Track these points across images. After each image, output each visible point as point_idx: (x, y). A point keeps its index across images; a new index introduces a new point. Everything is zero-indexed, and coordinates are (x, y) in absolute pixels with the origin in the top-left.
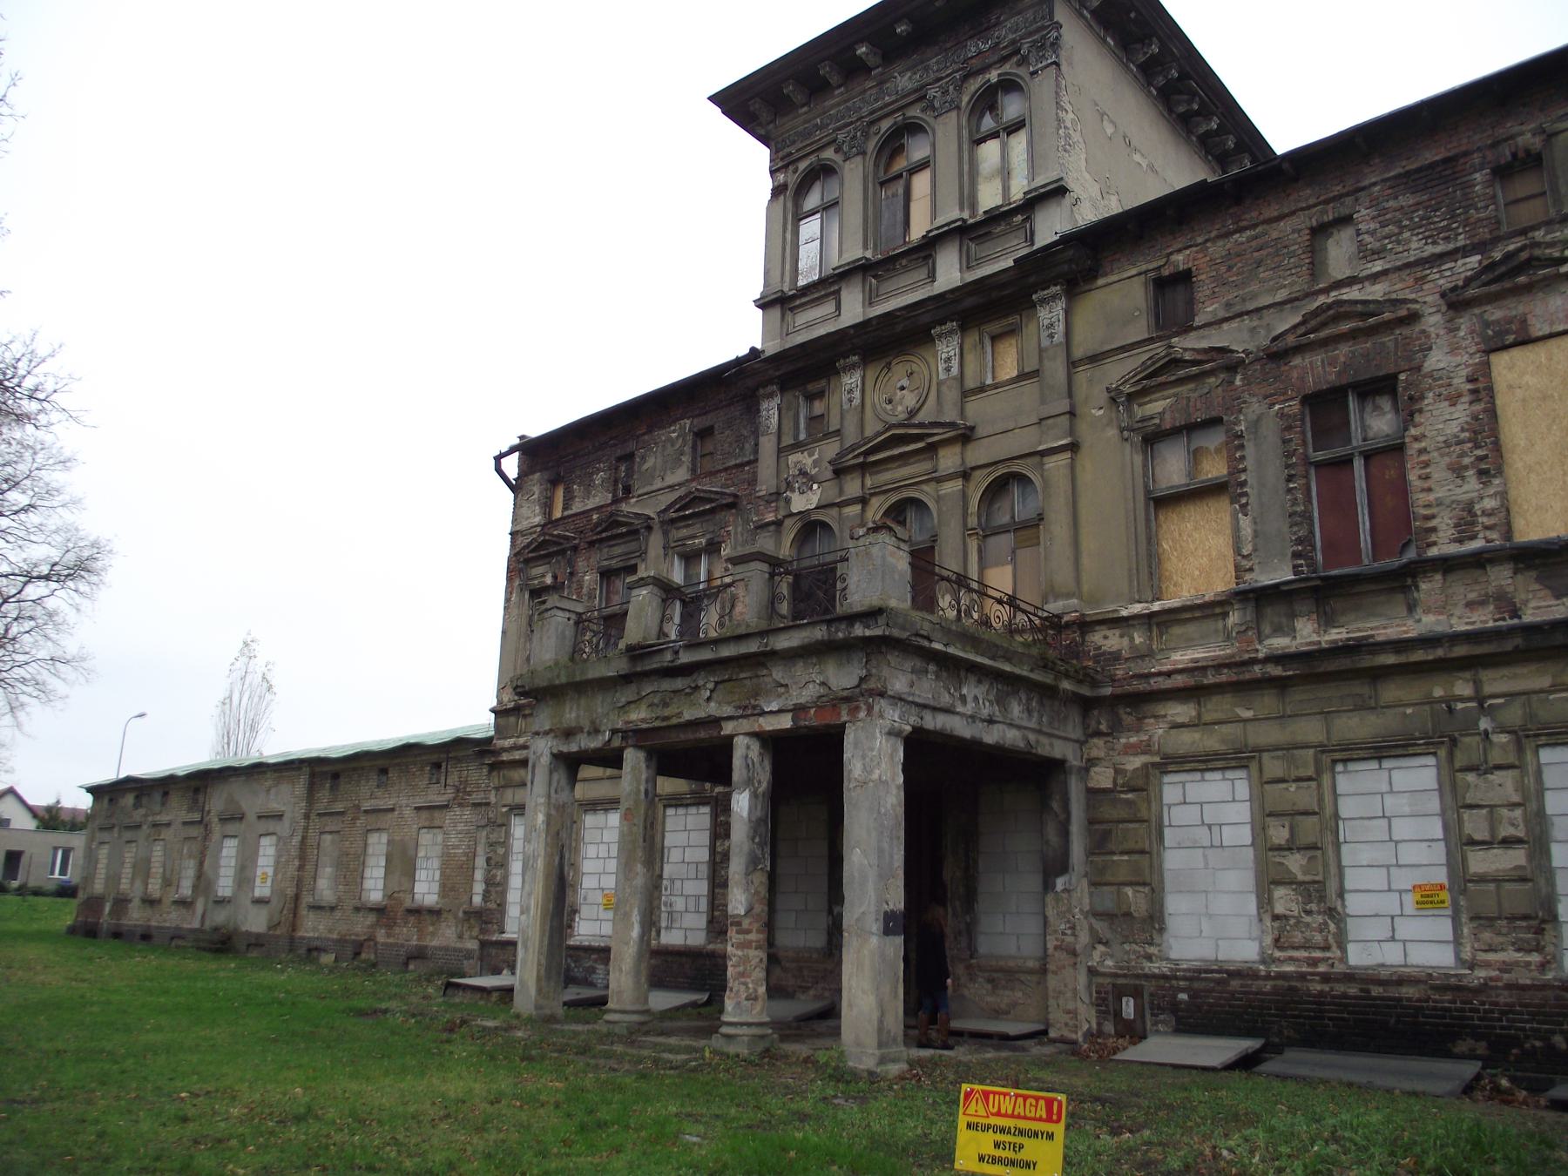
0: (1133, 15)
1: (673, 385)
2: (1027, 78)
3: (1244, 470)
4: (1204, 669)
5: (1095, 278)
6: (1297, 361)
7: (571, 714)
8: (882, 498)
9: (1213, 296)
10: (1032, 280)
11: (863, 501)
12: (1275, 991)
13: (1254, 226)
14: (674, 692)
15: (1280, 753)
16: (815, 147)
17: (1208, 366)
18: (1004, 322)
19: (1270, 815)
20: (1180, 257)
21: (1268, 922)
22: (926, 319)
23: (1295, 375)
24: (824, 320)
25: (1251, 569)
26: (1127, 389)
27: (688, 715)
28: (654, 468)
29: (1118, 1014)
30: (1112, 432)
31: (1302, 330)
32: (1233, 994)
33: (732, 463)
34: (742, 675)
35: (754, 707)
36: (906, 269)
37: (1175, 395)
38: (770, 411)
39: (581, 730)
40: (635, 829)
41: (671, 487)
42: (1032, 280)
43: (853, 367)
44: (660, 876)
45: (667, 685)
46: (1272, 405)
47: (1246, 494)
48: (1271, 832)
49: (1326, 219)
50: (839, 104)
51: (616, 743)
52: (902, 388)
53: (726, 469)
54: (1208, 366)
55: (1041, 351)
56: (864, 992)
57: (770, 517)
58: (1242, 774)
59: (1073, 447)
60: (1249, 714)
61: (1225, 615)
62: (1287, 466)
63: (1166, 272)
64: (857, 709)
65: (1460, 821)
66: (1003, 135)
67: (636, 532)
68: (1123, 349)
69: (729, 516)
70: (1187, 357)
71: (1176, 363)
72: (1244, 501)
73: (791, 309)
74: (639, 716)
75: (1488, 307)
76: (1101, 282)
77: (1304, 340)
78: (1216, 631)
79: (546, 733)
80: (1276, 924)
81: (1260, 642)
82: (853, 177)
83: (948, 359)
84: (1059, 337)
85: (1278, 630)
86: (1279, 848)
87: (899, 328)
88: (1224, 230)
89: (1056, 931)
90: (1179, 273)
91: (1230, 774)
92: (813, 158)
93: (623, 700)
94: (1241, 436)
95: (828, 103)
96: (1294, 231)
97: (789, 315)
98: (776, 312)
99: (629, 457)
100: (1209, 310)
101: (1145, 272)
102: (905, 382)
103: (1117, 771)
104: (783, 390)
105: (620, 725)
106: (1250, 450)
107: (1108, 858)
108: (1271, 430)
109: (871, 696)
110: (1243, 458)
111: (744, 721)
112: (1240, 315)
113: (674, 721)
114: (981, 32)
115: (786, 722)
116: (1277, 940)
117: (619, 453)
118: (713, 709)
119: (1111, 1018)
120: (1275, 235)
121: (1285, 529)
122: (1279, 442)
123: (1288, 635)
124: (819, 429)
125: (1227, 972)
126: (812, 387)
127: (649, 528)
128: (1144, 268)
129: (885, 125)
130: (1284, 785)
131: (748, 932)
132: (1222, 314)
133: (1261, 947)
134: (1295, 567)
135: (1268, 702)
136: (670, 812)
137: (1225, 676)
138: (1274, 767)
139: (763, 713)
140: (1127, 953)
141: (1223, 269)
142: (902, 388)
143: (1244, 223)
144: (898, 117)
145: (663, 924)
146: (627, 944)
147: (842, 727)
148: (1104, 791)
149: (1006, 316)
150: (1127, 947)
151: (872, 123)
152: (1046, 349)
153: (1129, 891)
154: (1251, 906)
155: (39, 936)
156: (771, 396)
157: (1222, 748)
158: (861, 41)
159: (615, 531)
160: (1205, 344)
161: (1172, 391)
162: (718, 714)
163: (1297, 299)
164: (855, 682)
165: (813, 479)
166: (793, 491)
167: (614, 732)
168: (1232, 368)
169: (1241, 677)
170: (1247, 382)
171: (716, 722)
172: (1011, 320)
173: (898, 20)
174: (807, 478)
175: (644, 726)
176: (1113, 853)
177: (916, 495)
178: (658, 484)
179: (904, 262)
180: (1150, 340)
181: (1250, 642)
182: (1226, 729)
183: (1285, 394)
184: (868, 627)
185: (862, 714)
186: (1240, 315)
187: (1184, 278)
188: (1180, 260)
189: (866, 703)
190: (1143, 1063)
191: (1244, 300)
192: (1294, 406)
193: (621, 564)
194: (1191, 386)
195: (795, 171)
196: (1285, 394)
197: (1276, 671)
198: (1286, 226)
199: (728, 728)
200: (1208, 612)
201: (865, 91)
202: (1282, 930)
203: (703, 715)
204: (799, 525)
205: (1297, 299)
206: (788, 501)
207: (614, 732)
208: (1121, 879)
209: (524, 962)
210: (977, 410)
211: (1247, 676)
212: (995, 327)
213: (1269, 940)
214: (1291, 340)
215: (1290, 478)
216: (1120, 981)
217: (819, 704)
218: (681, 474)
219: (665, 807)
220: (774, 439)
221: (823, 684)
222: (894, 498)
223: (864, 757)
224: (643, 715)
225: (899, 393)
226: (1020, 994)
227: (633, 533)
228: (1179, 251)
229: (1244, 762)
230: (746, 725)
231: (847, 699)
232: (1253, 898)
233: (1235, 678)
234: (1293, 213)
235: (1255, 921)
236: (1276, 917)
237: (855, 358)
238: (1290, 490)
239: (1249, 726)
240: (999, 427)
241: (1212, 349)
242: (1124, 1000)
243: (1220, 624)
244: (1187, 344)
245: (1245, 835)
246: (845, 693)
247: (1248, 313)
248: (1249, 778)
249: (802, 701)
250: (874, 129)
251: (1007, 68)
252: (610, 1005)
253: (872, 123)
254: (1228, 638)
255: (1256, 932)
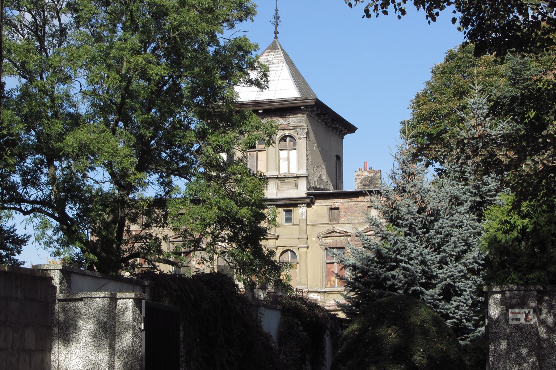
0: (209, 121)
1: (345, 120)
17: (342, 235)
20: (337, 204)
26: (322, 236)
30: (317, 245)
55: (299, 220)
59: (308, 248)
75: (279, 119)
84: (304, 217)
100: (342, 220)
132: (346, 222)
155: (100, 298)
244: (338, 228)
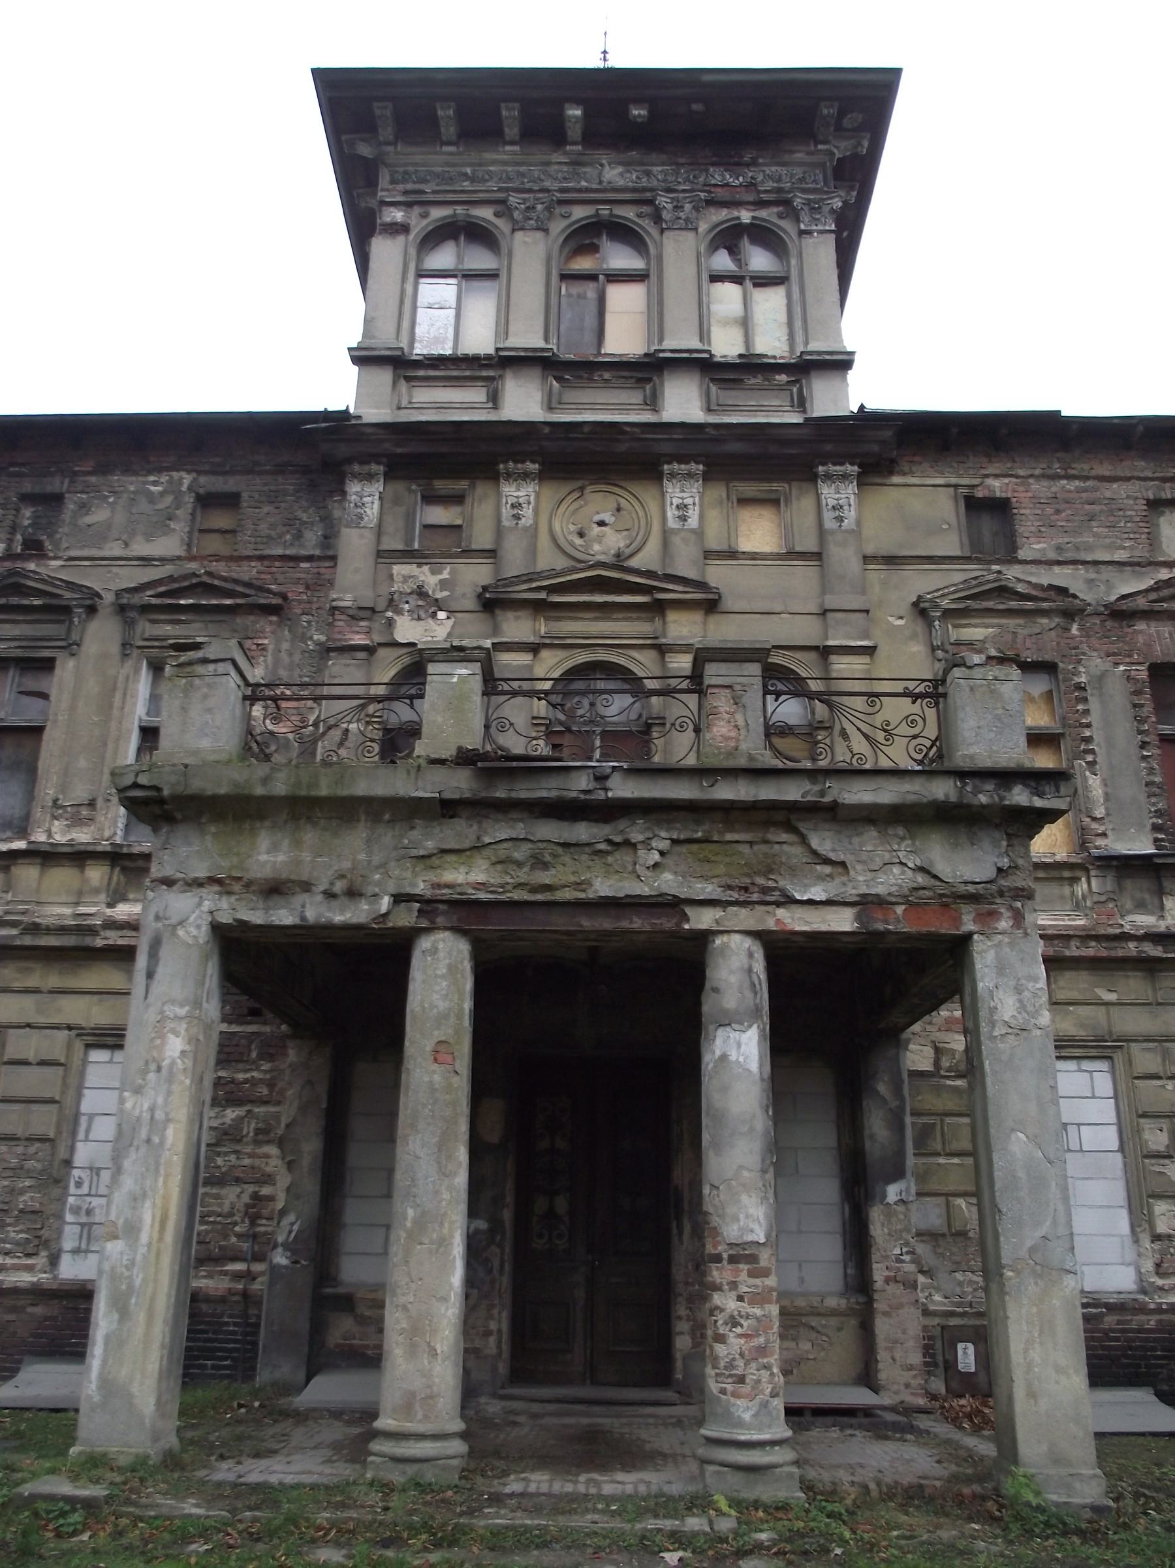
2: (794, 235)
3: (1089, 725)
4: (1068, 938)
5: (891, 473)
6: (1141, 626)
7: (268, 854)
8: (561, 654)
9: (1039, 534)
10: (828, 447)
11: (534, 649)
12: (1161, 1327)
13: (1087, 478)
14: (566, 845)
15: (1151, 1045)
16: (464, 197)
17: (1045, 605)
18: (765, 486)
19: (1144, 1115)
21: (1146, 1243)
22: (666, 448)
23: (1141, 639)
24: (470, 407)
25: (1104, 835)
26: (945, 603)
27: (603, 887)
28: (108, 525)
29: (950, 1366)
31: (1153, 596)
32: (1106, 1332)
33: (280, 552)
34: (729, 837)
35: (765, 890)
36: (607, 385)
37: (999, 626)
38: (367, 498)
39: (306, 887)
40: (456, 1080)
41: (146, 561)
42: (828, 447)
43: (525, 476)
44: (68, 1163)
45: (549, 830)
46: (1117, 664)
47: (1092, 752)
48: (1147, 1135)
49: (1164, 496)
50: (505, 163)
51: (406, 918)
52: (601, 524)
53: (261, 558)
54: (1045, 605)
56: (1059, 1370)
57: (359, 639)
58: (1103, 1065)
60: (1112, 997)
61: (1074, 880)
62: (1140, 732)
63: (979, 494)
64: (993, 915)
65: (1138, 1131)
66: (748, 284)
67: (66, 610)
68: (930, 559)
69: (266, 625)
70: (1020, 588)
71: (1003, 591)
72: (1090, 758)
73: (408, 379)
74: (470, 876)
76: (896, 479)
77: (1157, 606)
78: (1062, 897)
79: (198, 883)
80: (1157, 1246)
81: (1122, 916)
82: (530, 256)
83: (682, 507)
85: (1141, 907)
86: (1157, 1156)
87: (622, 447)
88: (1050, 472)
89: (886, 1257)
90: (995, 499)
91: (1087, 1065)
92: (460, 210)
93: (430, 845)
94: (1084, 689)
95: (488, 156)
96: (1128, 497)
97: (403, 386)
98: (384, 376)
99: (57, 500)
101: (956, 486)
102: (607, 517)
103: (938, 1051)
104: (388, 477)
105: (420, 887)
106: (1094, 705)
107: (931, 1160)
108: (1117, 693)
109: (1015, 898)
110: (1086, 712)
111: (744, 912)
112: (1074, 562)
113: (567, 895)
114: (734, 165)
115: (843, 921)
116: (1158, 1265)
117: (28, 487)
118: (668, 882)
119: (940, 1371)
120: (1108, 494)
121: (1142, 797)
122: (1129, 706)
123: (1152, 913)
124: (449, 544)
125: (1107, 1306)
126: (442, 486)
127: (92, 610)
128: (954, 481)
129: (580, 213)
130: (1159, 1083)
131: (765, 1273)
132: (1052, 555)
133: (1139, 1273)
134: (1156, 840)
135: (1134, 985)
136: (96, 1055)
137: (1092, 950)
138: (1146, 1059)
139: (789, 901)
140: (960, 1284)
141: (1049, 511)
142: (601, 524)
143: (1071, 472)
144: (604, 210)
145: (68, 1244)
146: (444, 1299)
147: (968, 937)
148: (922, 1074)
149: (769, 480)
150: (959, 1276)
151: (561, 202)
152: (832, 532)
153: (961, 1202)
154: (1124, 1226)
156: (370, 477)
157: (1082, 1033)
158: (577, 102)
159: (15, 600)
160: (1045, 582)
161: (996, 621)
162: (684, 893)
163: (1139, 564)
164: (991, 873)
165: (438, 605)
166: (399, 612)
167: (399, 899)
168: (1069, 615)
169: (1113, 953)
170: (1086, 632)
171: (675, 905)
172: (775, 486)
173: (638, 101)
174: (427, 603)
175: (483, 896)
176: (939, 1155)
177: (621, 661)
178: (116, 550)
179: (607, 375)
180: (966, 559)
181: (1111, 915)
182: (1083, 1011)
183: (1130, 656)
184: (1040, 795)
185: (1004, 924)
186: (1074, 562)
187: (1000, 508)
188: (997, 487)
189: (1011, 908)
190: (1143, 1434)
191: (1077, 549)
192: (1142, 672)
193: (19, 653)
194: (1021, 621)
195: (424, 216)
196: (1130, 656)
197: (1155, 951)
198: (1118, 490)
199: (703, 919)
200: (1055, 874)
201: (548, 164)
202: (1163, 1253)
203: (645, 890)
204: (407, 660)
205: (1139, 564)
206: (390, 623)
207: (399, 899)
208: (952, 1188)
209: (115, 1342)
210: (718, 575)
211: (1120, 953)
212: (749, 489)
213: (1148, 1265)
214: (1141, 603)
215: (1144, 745)
216: (953, 1322)
217: (912, 900)
218: (169, 545)
219: (88, 1046)
220: (369, 536)
221: (921, 869)
222: (582, 657)
223: (1018, 990)
224: (481, 877)
225: (597, 530)
226: (807, 1346)
227: (58, 611)
228: (997, 476)
229: (1108, 1052)
230: (745, 918)
231: (973, 898)
232: (1124, 1213)
233: (1104, 953)
234: (1128, 479)
235: (1128, 1241)
236: (1156, 1238)
237: (533, 467)
238: (1144, 758)
239: (1112, 1009)
240: (759, 606)
241: (1052, 587)
242: (960, 1346)
243: (1067, 890)
245: (1110, 1138)
246: (971, 889)
247: (1084, 563)
248: (1113, 1071)
249: (880, 890)
250: (564, 210)
251: (763, 213)
252: (384, 1422)
253: (561, 202)
254: (1077, 907)
255: (1130, 1255)
